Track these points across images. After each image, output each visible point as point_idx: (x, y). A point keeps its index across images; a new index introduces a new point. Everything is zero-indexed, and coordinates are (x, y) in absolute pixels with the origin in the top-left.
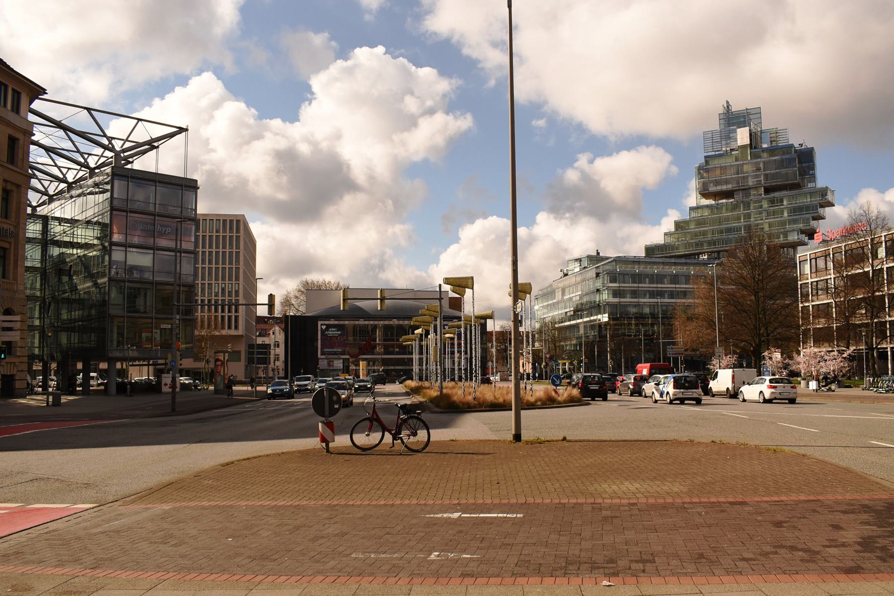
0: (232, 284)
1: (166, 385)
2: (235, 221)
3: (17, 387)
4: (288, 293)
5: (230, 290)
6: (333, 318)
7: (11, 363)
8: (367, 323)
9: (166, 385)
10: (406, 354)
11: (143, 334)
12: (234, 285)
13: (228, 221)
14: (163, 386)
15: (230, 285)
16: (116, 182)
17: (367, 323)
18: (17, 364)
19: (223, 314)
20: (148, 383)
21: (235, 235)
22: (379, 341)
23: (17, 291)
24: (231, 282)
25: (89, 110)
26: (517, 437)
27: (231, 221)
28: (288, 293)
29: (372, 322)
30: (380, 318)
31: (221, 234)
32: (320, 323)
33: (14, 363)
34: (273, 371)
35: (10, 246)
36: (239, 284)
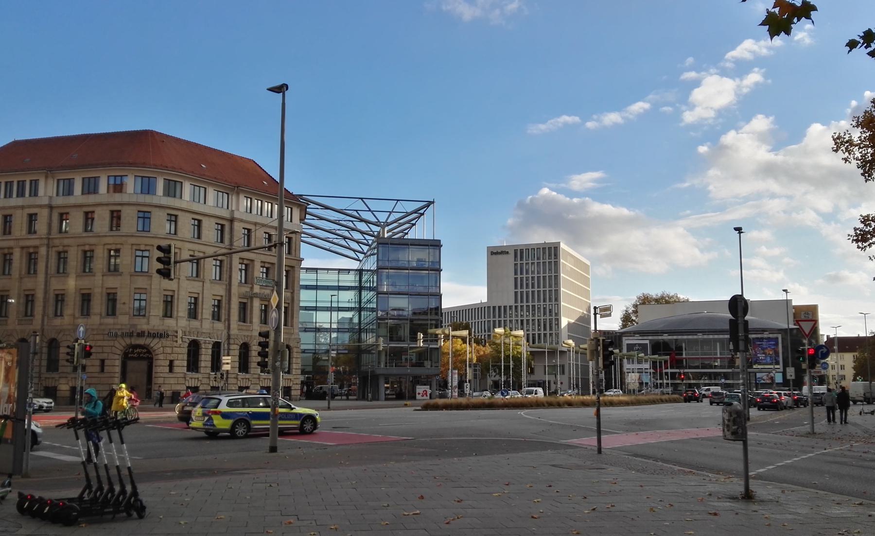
0: (552, 304)
1: (419, 394)
2: (553, 248)
3: (292, 394)
4: (627, 308)
5: (550, 308)
6: (666, 333)
7: (288, 379)
8: (670, 337)
9: (419, 394)
10: (725, 369)
11: (403, 356)
12: (553, 305)
13: (547, 248)
14: (417, 395)
15: (550, 306)
16: (380, 249)
17: (670, 337)
18: (292, 380)
19: (545, 332)
20: (770, 383)
21: (553, 260)
22: (686, 355)
23: (293, 334)
24: (551, 303)
25: (362, 199)
26: (600, 451)
27: (550, 248)
28: (627, 308)
29: (675, 337)
30: (709, 332)
31: (541, 261)
32: (624, 338)
33: (290, 379)
34: (554, 383)
35: (289, 305)
36: (558, 304)
